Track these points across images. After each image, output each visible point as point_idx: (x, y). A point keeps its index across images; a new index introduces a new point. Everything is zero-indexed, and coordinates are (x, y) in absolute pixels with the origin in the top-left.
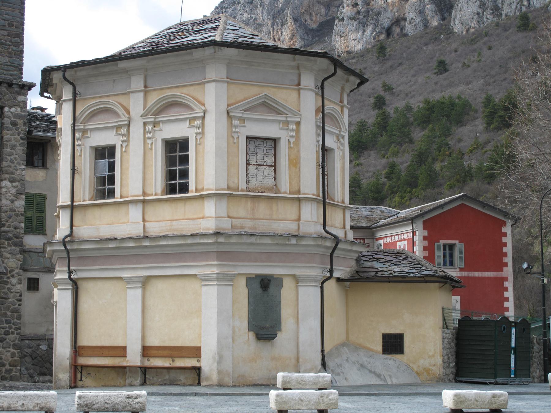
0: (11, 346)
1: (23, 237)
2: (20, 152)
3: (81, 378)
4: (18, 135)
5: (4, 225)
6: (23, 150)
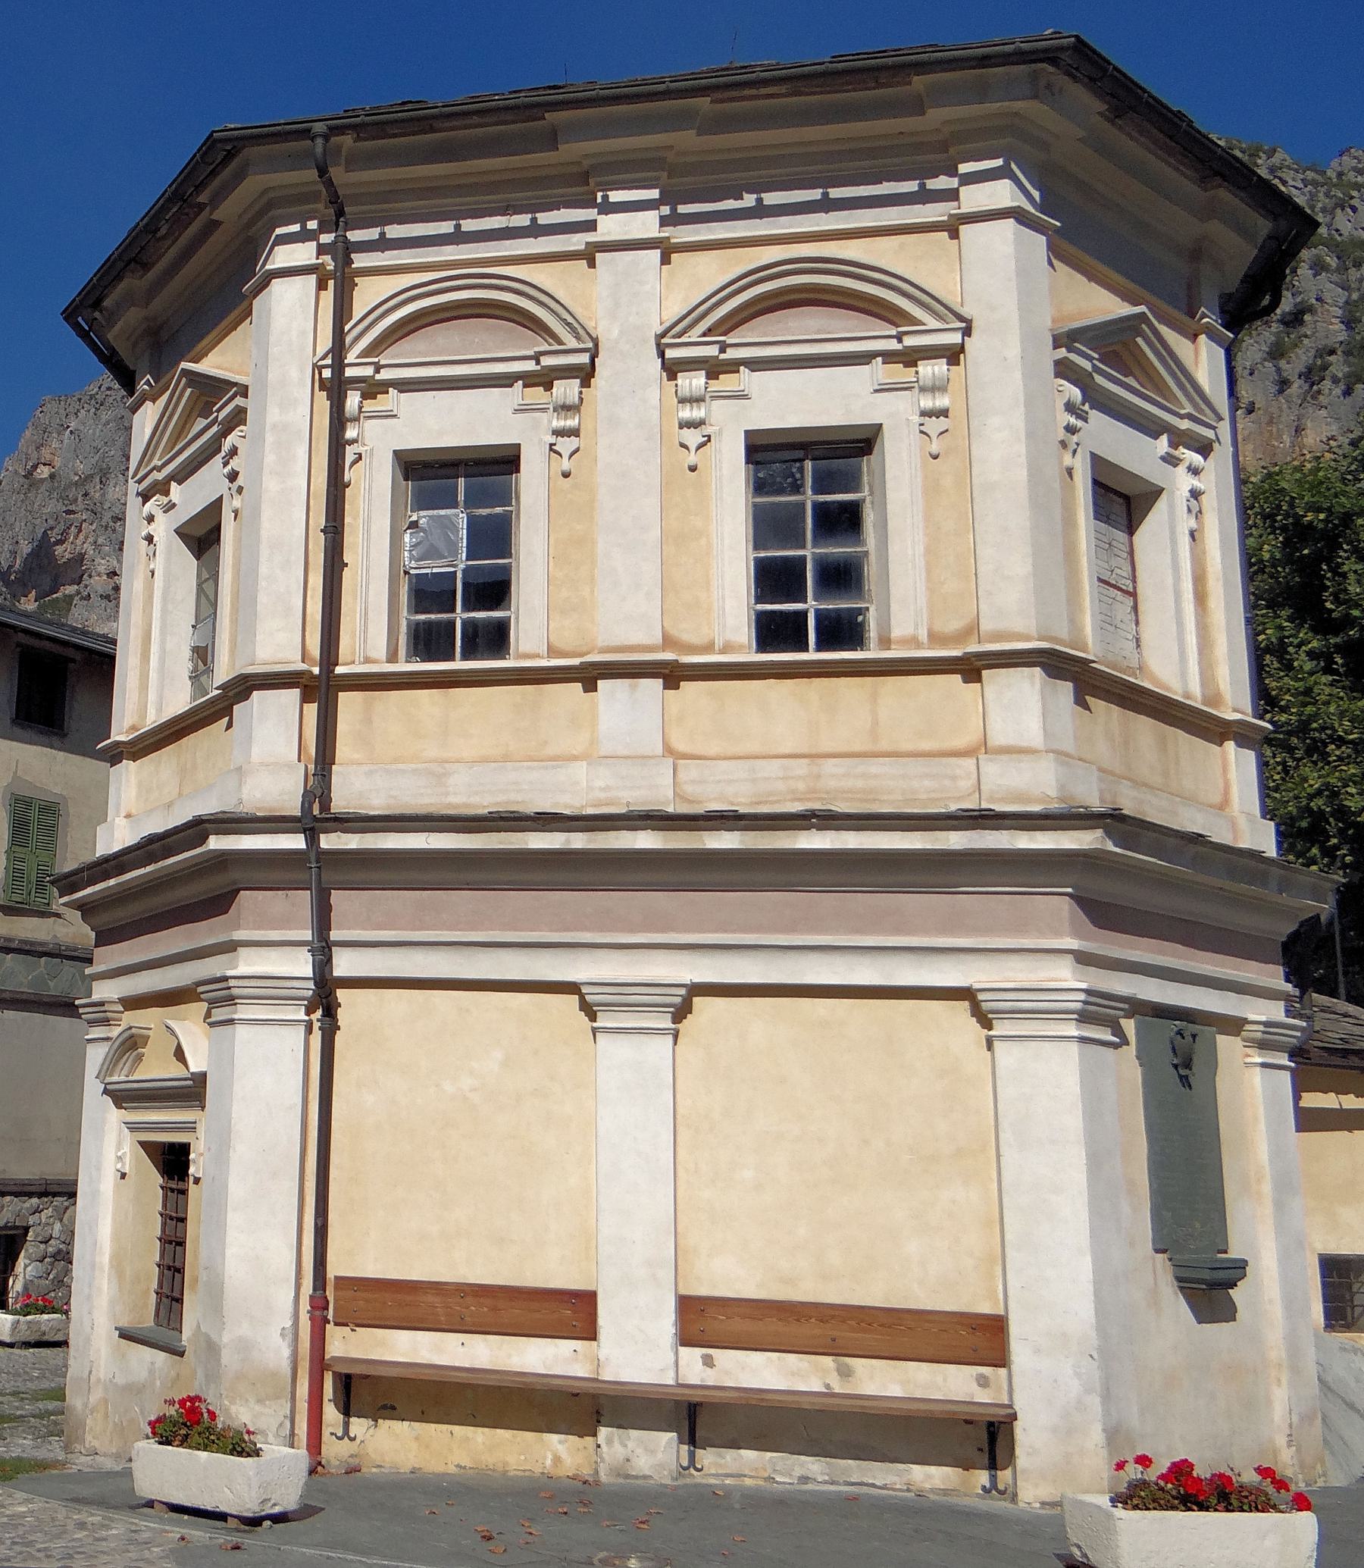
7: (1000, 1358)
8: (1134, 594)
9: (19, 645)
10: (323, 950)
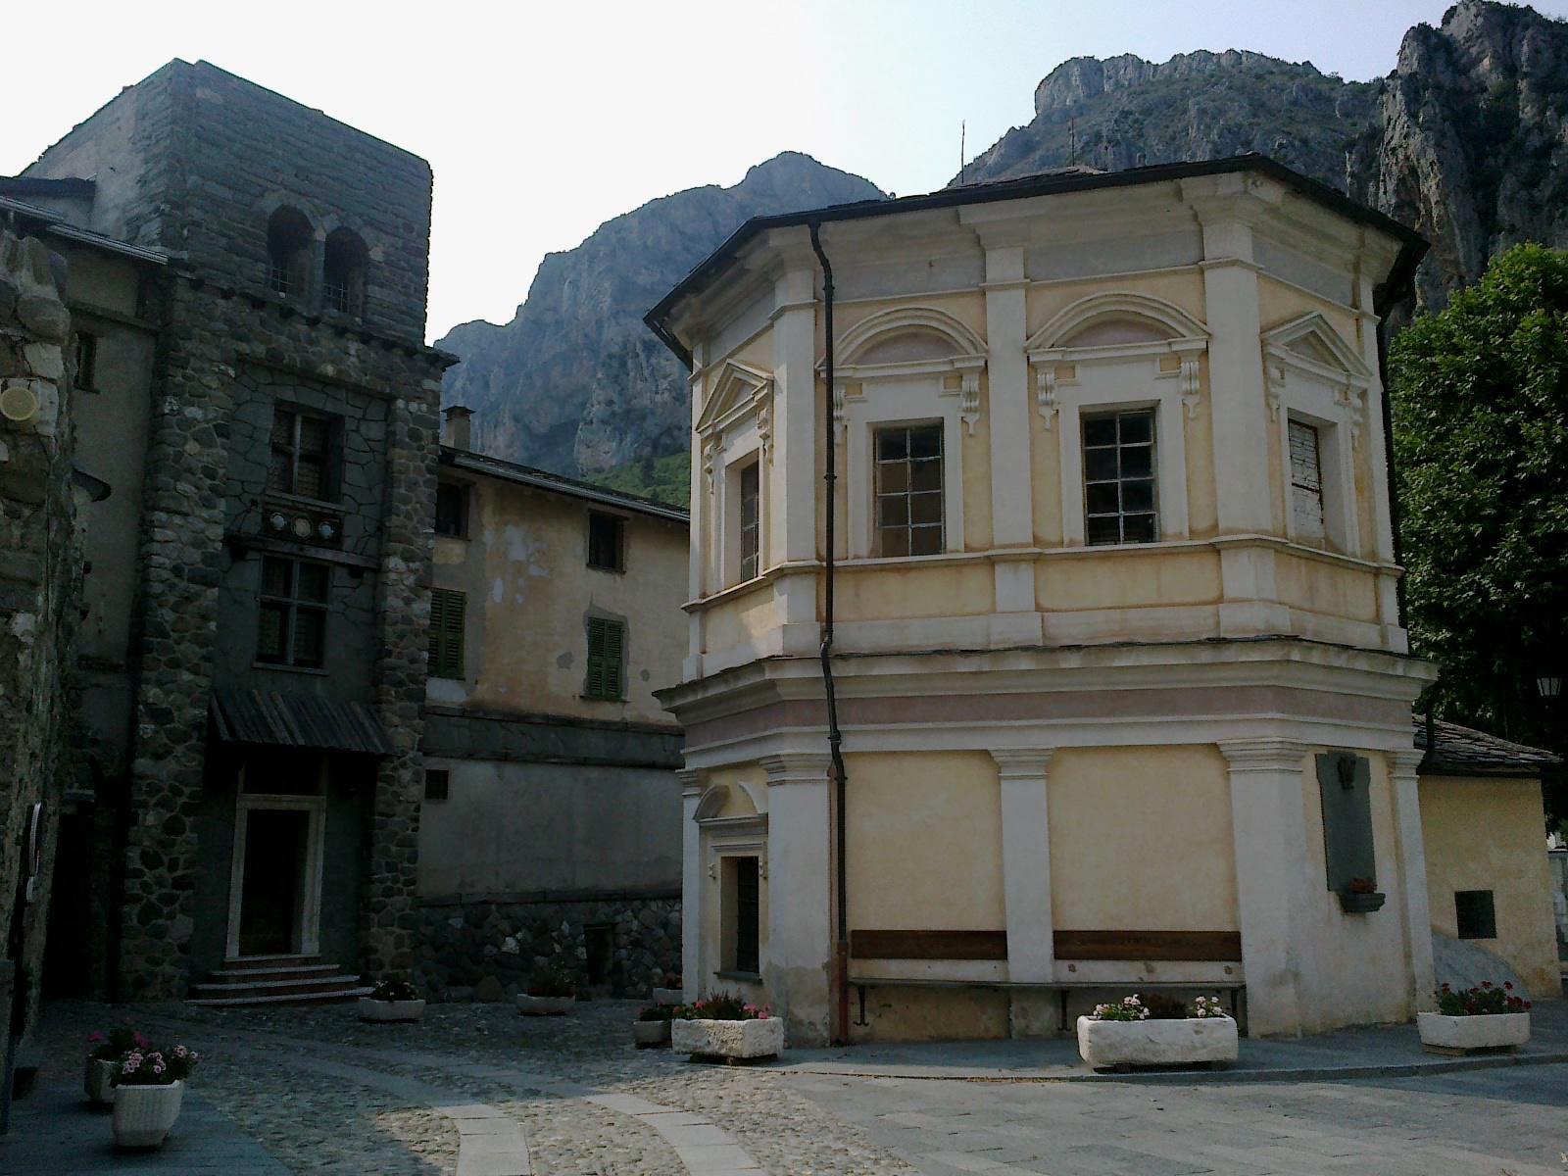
0: (396, 923)
1: (426, 680)
2: (423, 499)
3: (863, 1017)
4: (423, 462)
5: (389, 654)
6: (430, 495)
7: (1237, 956)
8: (1319, 492)
9: (589, 510)
10: (836, 738)
